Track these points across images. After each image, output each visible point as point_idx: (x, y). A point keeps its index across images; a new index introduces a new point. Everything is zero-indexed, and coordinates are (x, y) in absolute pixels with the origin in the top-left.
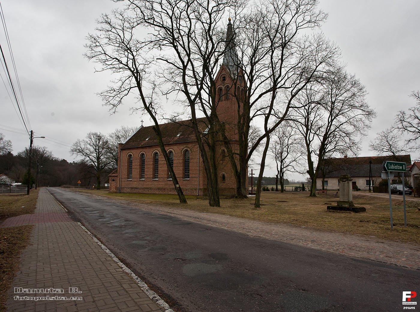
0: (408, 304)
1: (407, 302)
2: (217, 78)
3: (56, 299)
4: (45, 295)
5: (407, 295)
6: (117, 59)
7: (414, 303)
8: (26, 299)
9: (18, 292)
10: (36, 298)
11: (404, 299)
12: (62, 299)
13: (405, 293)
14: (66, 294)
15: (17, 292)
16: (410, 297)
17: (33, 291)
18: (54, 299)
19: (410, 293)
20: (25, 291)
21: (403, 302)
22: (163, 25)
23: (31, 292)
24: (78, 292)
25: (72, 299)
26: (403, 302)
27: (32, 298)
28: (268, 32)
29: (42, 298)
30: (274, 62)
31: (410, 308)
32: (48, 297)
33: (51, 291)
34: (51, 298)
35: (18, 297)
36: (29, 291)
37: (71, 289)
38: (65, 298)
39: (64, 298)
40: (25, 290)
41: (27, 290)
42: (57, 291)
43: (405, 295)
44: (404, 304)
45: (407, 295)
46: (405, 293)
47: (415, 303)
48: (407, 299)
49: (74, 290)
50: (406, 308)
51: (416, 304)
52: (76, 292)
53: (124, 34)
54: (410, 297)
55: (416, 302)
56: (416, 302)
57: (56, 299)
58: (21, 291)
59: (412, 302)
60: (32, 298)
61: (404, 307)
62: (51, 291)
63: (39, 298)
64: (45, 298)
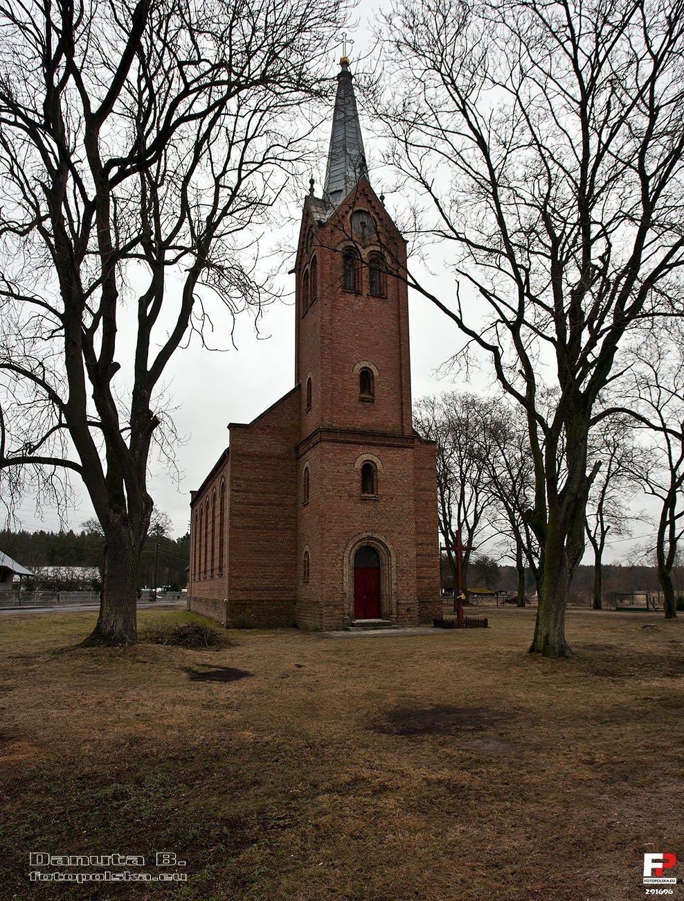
0: (656, 883)
1: (655, 879)
2: (301, 247)
3: (127, 877)
4: (101, 870)
5: (654, 861)
6: (268, 205)
7: (669, 879)
8: (57, 878)
9: (38, 864)
10: (80, 877)
11: (647, 872)
12: (141, 878)
13: (648, 857)
14: (150, 867)
15: (36, 863)
16: (660, 865)
17: (74, 861)
18: (121, 878)
19: (660, 856)
20: (55, 862)
21: (644, 879)
22: (517, 91)
23: (70, 864)
24: (177, 862)
25: (162, 878)
26: (644, 879)
27: (97, 877)
28: (247, 51)
29: (94, 877)
30: (532, 203)
31: (661, 892)
32: (108, 874)
33: (116, 861)
34: (115, 877)
35: (38, 874)
36: (65, 861)
37: (161, 858)
38: (148, 877)
39: (144, 876)
40: (54, 858)
41: (60, 858)
42: (130, 862)
43: (650, 862)
44: (646, 883)
45: (654, 861)
46: (648, 857)
47: (673, 881)
48: (654, 870)
49: (167, 857)
50: (653, 891)
51: (675, 883)
52: (172, 862)
53: (460, 134)
54: (660, 865)
55: (675, 879)
56: (675, 879)
57: (127, 877)
58: (46, 861)
59: (667, 879)
60: (97, 877)
61: (648, 890)
62: (116, 861)
63: (88, 878)
64: (102, 877)
